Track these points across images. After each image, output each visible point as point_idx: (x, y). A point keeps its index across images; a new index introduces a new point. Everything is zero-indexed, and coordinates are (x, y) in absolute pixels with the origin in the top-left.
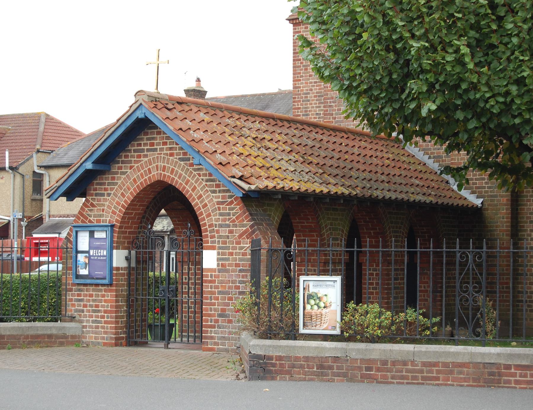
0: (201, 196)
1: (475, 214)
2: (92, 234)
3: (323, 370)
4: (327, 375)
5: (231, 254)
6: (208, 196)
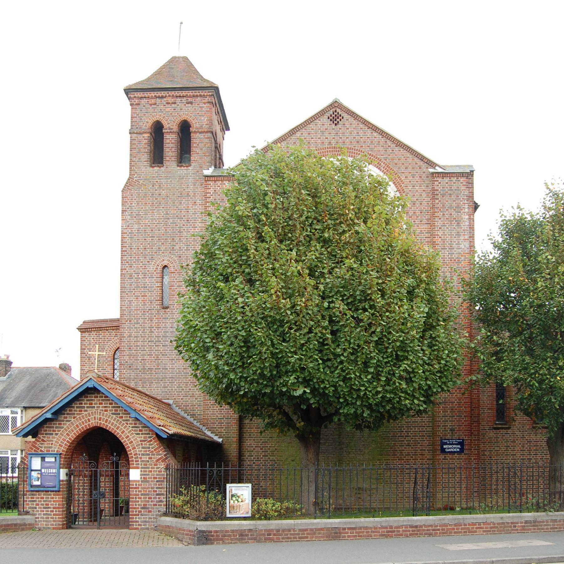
0: (67, 434)
1: (217, 447)
2: (43, 459)
3: (242, 537)
4: (245, 539)
5: (151, 471)
6: (134, 437)
